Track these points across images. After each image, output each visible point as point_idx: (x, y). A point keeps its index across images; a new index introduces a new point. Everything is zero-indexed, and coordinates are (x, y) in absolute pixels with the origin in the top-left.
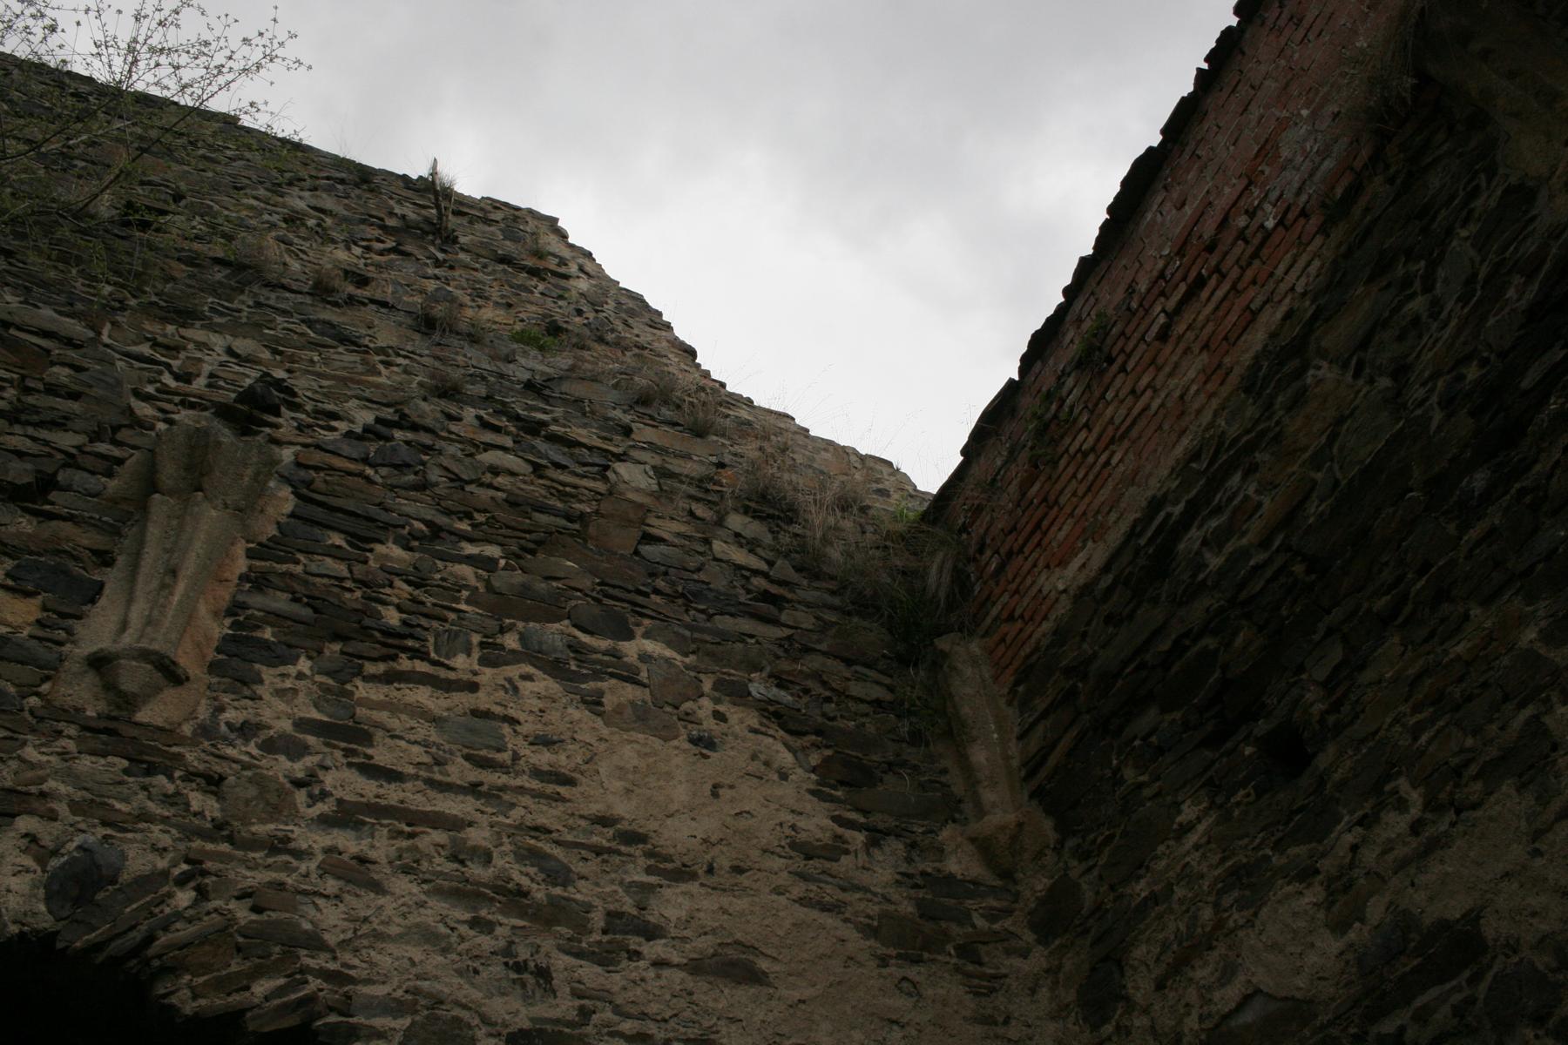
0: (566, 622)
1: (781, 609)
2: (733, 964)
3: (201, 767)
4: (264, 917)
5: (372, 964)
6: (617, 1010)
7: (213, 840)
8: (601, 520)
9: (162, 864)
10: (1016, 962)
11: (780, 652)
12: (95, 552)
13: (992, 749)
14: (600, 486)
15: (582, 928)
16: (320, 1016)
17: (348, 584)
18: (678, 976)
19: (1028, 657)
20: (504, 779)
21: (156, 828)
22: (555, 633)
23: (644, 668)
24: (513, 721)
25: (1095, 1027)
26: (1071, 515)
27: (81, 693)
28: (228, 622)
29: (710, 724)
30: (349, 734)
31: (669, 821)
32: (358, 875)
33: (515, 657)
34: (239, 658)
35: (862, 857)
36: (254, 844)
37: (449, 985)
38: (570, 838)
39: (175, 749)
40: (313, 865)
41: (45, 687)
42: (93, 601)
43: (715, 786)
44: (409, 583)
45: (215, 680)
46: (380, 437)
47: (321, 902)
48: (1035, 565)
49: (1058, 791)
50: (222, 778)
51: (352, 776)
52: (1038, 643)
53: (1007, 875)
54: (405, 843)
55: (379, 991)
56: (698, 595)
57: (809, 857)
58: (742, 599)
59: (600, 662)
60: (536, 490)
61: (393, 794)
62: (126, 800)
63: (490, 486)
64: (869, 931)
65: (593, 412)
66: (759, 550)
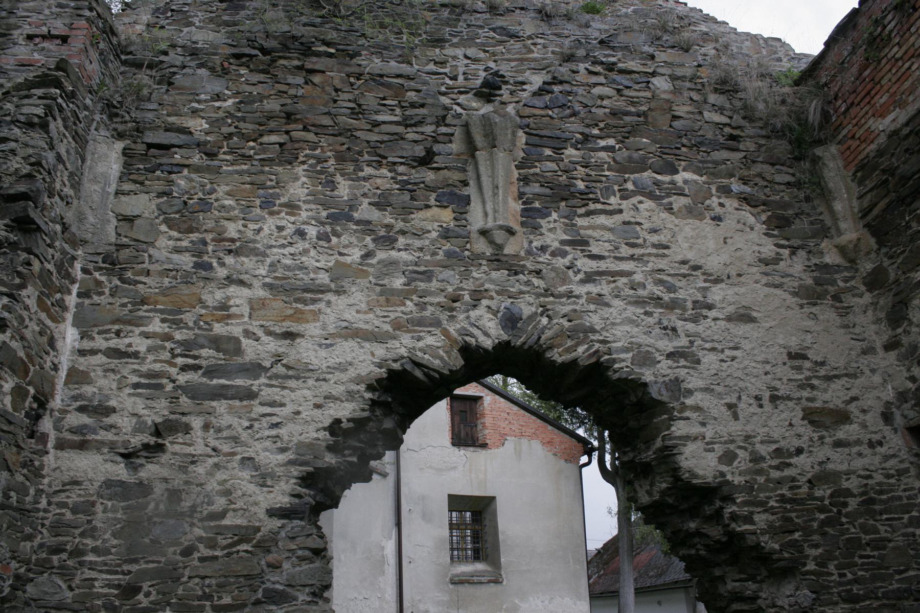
0: (650, 171)
1: (739, 142)
2: (743, 315)
3: (533, 268)
4: (572, 323)
5: (614, 335)
6: (703, 340)
7: (546, 296)
8: (654, 113)
9: (534, 309)
10: (857, 300)
11: (742, 166)
12: (461, 182)
13: (844, 201)
14: (648, 94)
15: (684, 309)
16: (602, 356)
17: (560, 173)
18: (723, 323)
19: (862, 160)
20: (642, 251)
21: (527, 296)
22: (647, 176)
23: (686, 187)
24: (639, 224)
25: (893, 329)
26: (888, 91)
27: (481, 246)
28: (520, 202)
29: (718, 210)
30: (580, 243)
31: (709, 258)
32: (599, 300)
33: (634, 193)
34: (531, 217)
35: (789, 261)
36: (560, 296)
37: (643, 339)
38: (672, 272)
39: (522, 263)
40: (584, 300)
41: (468, 246)
42: (469, 204)
43: (725, 238)
44: (583, 166)
45: (525, 230)
46: (548, 92)
47: (590, 314)
48: (867, 113)
49: (880, 228)
50: (541, 271)
51: (586, 260)
52: (868, 154)
53: (852, 261)
54: (613, 285)
55: (619, 344)
56: (701, 143)
57: (767, 265)
58: (721, 141)
59: (668, 188)
60: (621, 104)
61: (603, 265)
62: (513, 287)
63: (601, 106)
64: (795, 294)
65: (635, 51)
66: (725, 112)
